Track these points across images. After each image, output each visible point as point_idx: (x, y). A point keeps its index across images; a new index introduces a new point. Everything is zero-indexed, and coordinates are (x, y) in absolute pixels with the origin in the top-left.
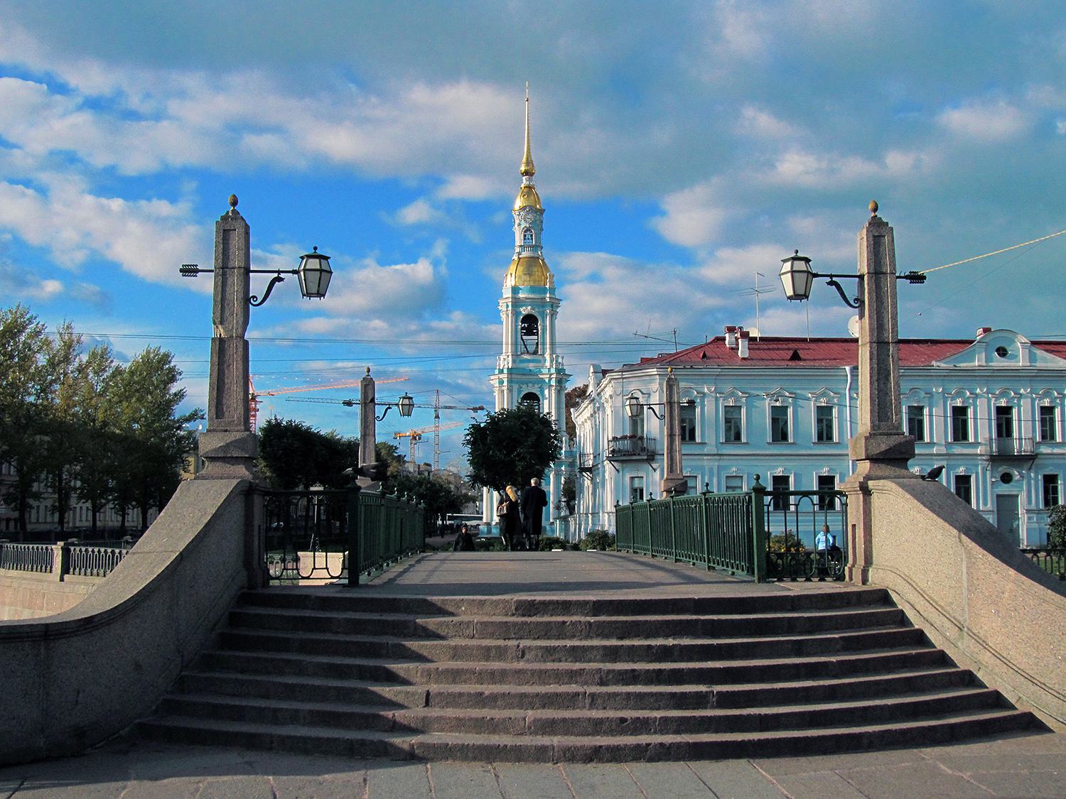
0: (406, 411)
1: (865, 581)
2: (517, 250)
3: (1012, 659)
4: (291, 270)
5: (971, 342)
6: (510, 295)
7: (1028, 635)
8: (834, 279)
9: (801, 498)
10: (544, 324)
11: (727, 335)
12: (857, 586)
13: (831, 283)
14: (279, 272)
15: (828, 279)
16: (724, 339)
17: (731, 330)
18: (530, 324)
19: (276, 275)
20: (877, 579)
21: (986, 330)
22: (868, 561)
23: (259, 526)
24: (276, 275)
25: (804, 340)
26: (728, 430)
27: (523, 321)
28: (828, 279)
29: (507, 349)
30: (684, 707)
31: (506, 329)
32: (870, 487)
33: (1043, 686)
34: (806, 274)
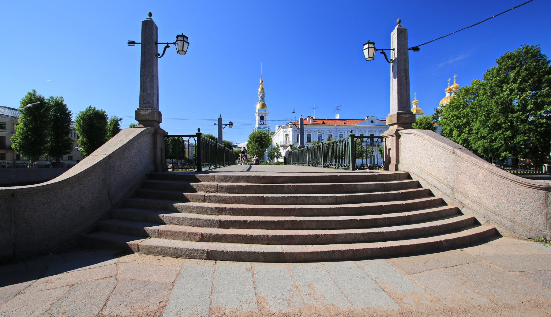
1: (397, 169)
2: (259, 101)
3: (482, 203)
4: (172, 42)
5: (364, 120)
6: (258, 111)
7: (493, 193)
8: (384, 51)
9: (367, 139)
10: (265, 118)
11: (308, 118)
13: (382, 53)
14: (168, 44)
15: (381, 51)
16: (307, 119)
17: (308, 117)
18: (262, 118)
19: (166, 45)
20: (402, 169)
21: (368, 117)
22: (398, 161)
23: (161, 149)
24: (166, 45)
25: (325, 119)
26: (308, 139)
27: (260, 117)
28: (381, 51)
29: (257, 123)
31: (257, 118)
32: (399, 133)
33: (502, 216)
34: (374, 49)
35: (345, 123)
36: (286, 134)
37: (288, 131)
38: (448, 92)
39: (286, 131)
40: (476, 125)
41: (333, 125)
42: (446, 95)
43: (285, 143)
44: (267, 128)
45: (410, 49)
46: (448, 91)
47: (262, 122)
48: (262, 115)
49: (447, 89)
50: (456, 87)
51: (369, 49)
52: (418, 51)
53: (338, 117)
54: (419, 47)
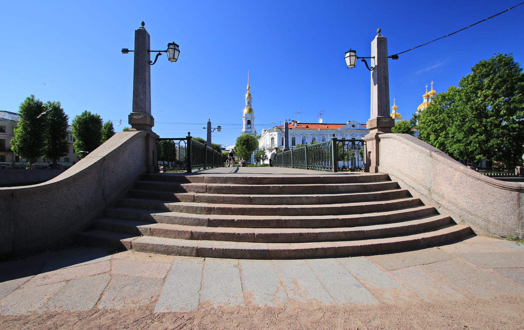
0: (219, 130)
1: (377, 171)
2: (246, 106)
3: (458, 204)
4: (164, 50)
6: (245, 116)
7: (468, 194)
8: (364, 59)
10: (252, 122)
12: (372, 172)
13: (363, 61)
14: (160, 51)
15: (362, 59)
16: (291, 123)
17: (293, 121)
18: (249, 122)
19: (158, 53)
20: (382, 171)
21: (349, 122)
22: (378, 164)
24: (158, 53)
26: (292, 142)
28: (362, 59)
29: (244, 127)
30: (233, 178)
32: (379, 137)
35: (327, 127)
36: (272, 137)
37: (273, 135)
38: (426, 98)
39: (272, 135)
40: (452, 129)
41: (317, 129)
42: (423, 101)
43: (270, 146)
44: (254, 132)
45: (389, 57)
46: (425, 97)
47: (249, 126)
48: (249, 119)
49: (425, 95)
50: (433, 93)
51: (351, 57)
52: (397, 59)
53: (321, 121)
54: (398, 55)
